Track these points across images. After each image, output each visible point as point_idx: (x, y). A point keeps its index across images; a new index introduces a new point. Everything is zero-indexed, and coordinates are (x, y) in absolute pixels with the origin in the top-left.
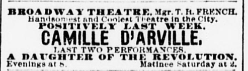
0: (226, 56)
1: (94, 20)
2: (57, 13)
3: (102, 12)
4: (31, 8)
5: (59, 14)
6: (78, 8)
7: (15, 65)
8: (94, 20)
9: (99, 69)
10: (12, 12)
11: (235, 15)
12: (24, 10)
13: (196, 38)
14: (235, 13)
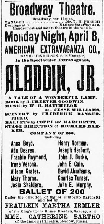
0: (49, 126)
2: (74, 102)
4: (59, 132)
6: (54, 132)
7: (8, 26)
11: (41, 107)
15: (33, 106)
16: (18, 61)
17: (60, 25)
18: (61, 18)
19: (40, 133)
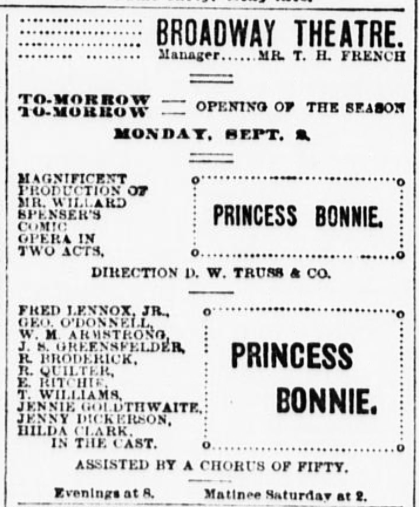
5: (139, 115)
10: (401, 106)
11: (327, 61)
12: (111, 97)
13: (366, 401)
14: (327, 57)
15: (217, 275)
16: (95, 97)
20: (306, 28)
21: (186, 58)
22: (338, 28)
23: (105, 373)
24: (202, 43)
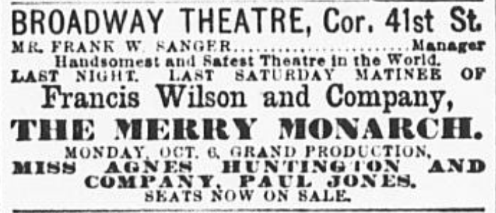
1: (307, 74)
3: (452, 127)
8: (307, 74)
9: (366, 3)
13: (299, 19)
17: (65, 153)
18: (95, 123)
19: (28, 164)
20: (194, 17)
21: (444, 49)
22: (232, 16)
23: (69, 49)
24: (132, 31)
